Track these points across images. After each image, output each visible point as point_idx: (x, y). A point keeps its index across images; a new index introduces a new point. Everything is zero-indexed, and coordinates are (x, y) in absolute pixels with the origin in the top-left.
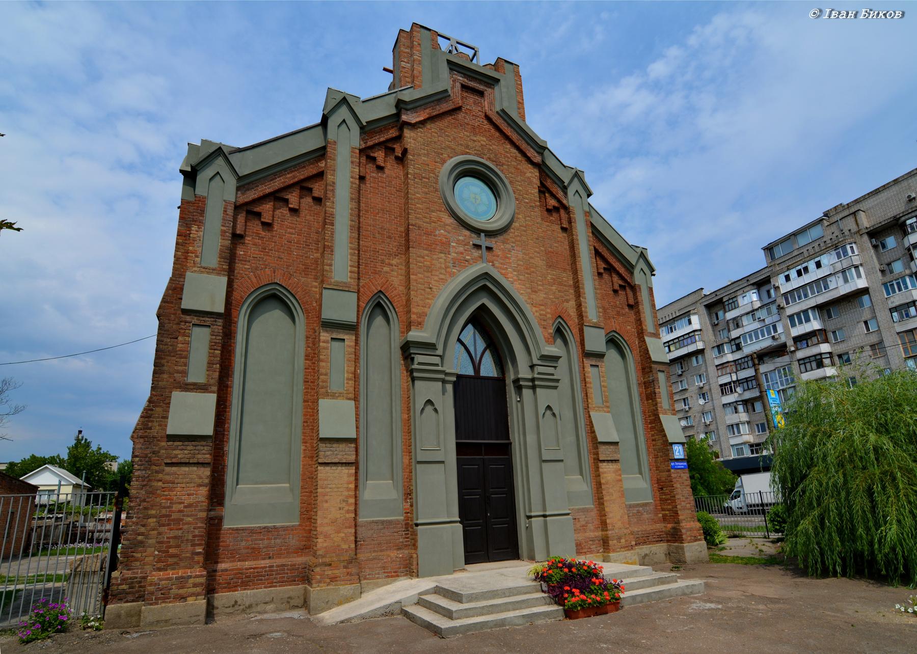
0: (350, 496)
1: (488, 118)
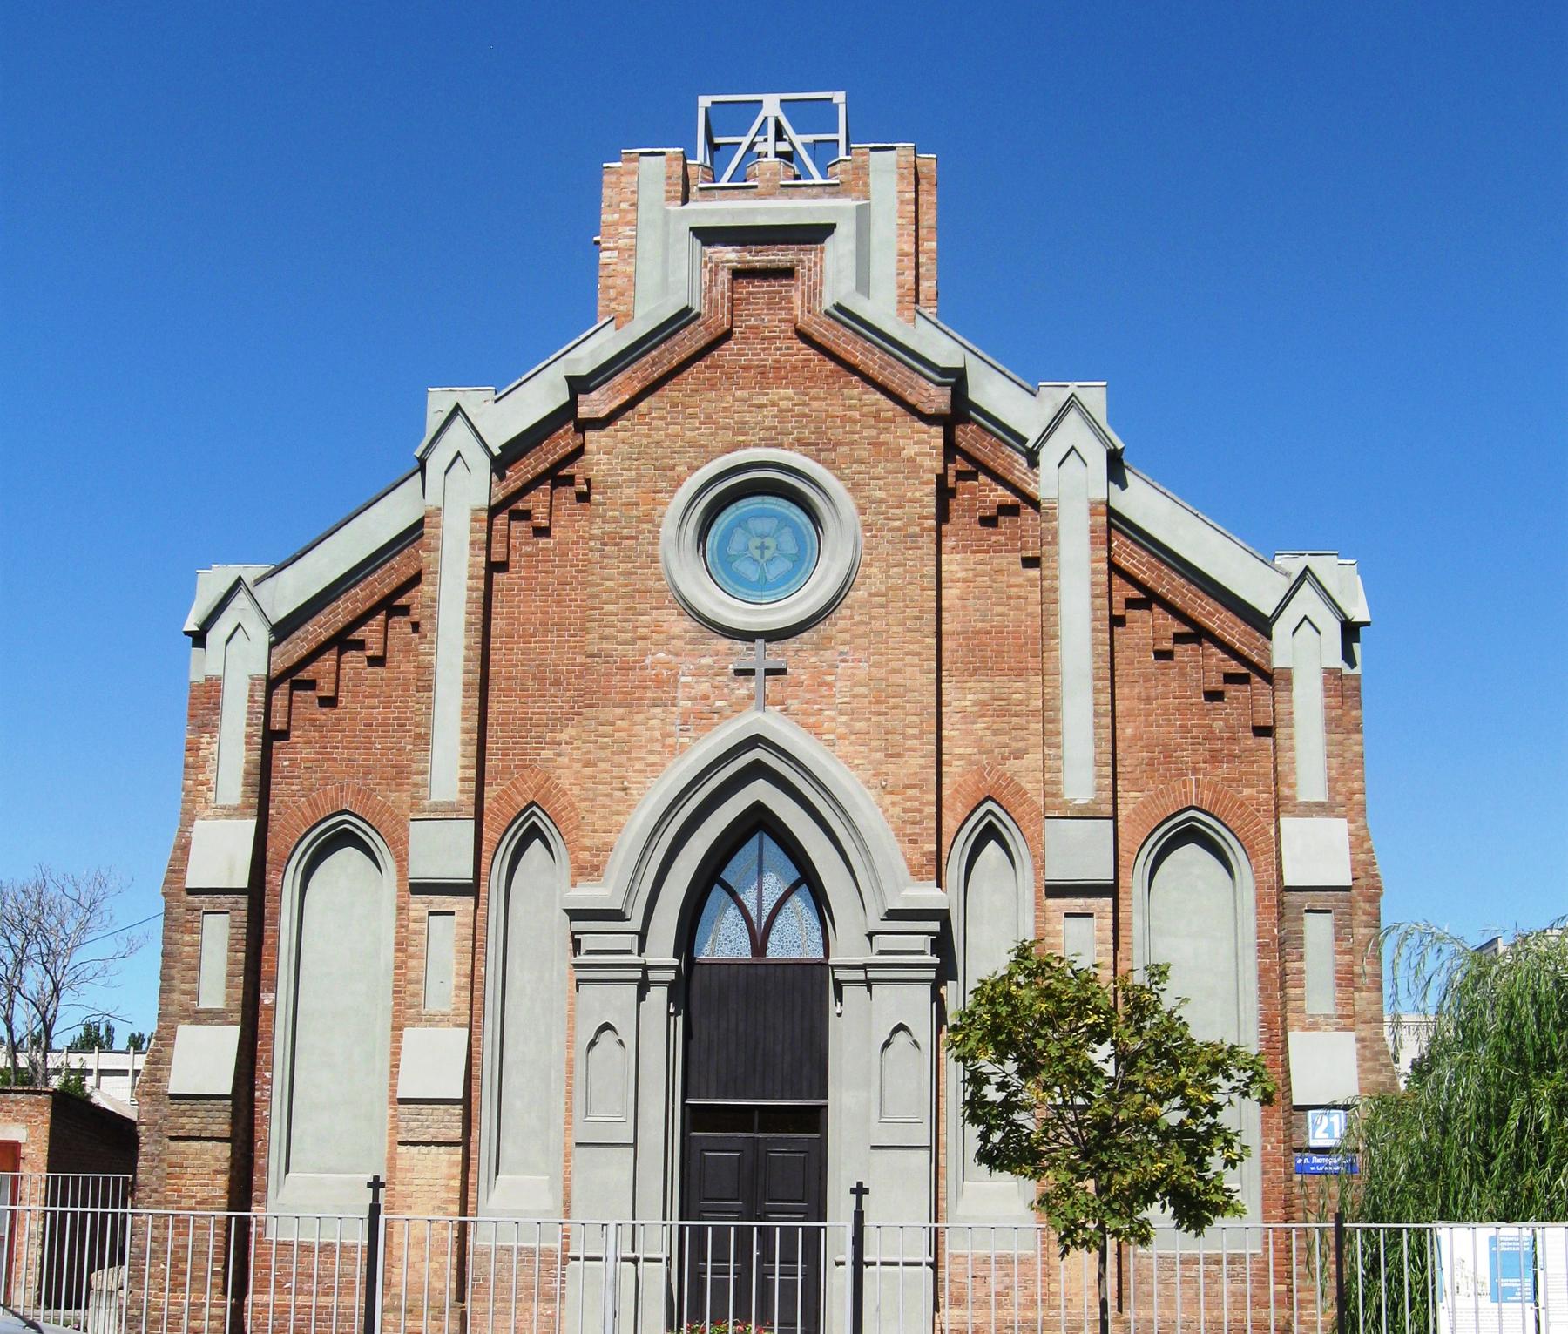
0: (449, 1201)
1: (803, 336)
